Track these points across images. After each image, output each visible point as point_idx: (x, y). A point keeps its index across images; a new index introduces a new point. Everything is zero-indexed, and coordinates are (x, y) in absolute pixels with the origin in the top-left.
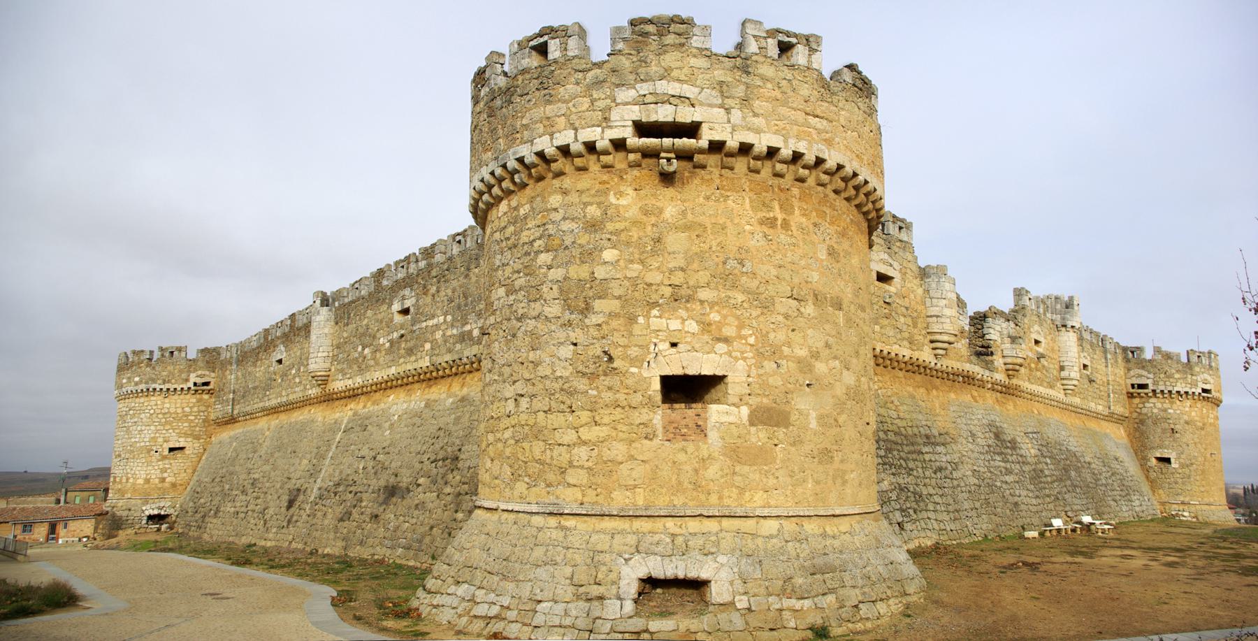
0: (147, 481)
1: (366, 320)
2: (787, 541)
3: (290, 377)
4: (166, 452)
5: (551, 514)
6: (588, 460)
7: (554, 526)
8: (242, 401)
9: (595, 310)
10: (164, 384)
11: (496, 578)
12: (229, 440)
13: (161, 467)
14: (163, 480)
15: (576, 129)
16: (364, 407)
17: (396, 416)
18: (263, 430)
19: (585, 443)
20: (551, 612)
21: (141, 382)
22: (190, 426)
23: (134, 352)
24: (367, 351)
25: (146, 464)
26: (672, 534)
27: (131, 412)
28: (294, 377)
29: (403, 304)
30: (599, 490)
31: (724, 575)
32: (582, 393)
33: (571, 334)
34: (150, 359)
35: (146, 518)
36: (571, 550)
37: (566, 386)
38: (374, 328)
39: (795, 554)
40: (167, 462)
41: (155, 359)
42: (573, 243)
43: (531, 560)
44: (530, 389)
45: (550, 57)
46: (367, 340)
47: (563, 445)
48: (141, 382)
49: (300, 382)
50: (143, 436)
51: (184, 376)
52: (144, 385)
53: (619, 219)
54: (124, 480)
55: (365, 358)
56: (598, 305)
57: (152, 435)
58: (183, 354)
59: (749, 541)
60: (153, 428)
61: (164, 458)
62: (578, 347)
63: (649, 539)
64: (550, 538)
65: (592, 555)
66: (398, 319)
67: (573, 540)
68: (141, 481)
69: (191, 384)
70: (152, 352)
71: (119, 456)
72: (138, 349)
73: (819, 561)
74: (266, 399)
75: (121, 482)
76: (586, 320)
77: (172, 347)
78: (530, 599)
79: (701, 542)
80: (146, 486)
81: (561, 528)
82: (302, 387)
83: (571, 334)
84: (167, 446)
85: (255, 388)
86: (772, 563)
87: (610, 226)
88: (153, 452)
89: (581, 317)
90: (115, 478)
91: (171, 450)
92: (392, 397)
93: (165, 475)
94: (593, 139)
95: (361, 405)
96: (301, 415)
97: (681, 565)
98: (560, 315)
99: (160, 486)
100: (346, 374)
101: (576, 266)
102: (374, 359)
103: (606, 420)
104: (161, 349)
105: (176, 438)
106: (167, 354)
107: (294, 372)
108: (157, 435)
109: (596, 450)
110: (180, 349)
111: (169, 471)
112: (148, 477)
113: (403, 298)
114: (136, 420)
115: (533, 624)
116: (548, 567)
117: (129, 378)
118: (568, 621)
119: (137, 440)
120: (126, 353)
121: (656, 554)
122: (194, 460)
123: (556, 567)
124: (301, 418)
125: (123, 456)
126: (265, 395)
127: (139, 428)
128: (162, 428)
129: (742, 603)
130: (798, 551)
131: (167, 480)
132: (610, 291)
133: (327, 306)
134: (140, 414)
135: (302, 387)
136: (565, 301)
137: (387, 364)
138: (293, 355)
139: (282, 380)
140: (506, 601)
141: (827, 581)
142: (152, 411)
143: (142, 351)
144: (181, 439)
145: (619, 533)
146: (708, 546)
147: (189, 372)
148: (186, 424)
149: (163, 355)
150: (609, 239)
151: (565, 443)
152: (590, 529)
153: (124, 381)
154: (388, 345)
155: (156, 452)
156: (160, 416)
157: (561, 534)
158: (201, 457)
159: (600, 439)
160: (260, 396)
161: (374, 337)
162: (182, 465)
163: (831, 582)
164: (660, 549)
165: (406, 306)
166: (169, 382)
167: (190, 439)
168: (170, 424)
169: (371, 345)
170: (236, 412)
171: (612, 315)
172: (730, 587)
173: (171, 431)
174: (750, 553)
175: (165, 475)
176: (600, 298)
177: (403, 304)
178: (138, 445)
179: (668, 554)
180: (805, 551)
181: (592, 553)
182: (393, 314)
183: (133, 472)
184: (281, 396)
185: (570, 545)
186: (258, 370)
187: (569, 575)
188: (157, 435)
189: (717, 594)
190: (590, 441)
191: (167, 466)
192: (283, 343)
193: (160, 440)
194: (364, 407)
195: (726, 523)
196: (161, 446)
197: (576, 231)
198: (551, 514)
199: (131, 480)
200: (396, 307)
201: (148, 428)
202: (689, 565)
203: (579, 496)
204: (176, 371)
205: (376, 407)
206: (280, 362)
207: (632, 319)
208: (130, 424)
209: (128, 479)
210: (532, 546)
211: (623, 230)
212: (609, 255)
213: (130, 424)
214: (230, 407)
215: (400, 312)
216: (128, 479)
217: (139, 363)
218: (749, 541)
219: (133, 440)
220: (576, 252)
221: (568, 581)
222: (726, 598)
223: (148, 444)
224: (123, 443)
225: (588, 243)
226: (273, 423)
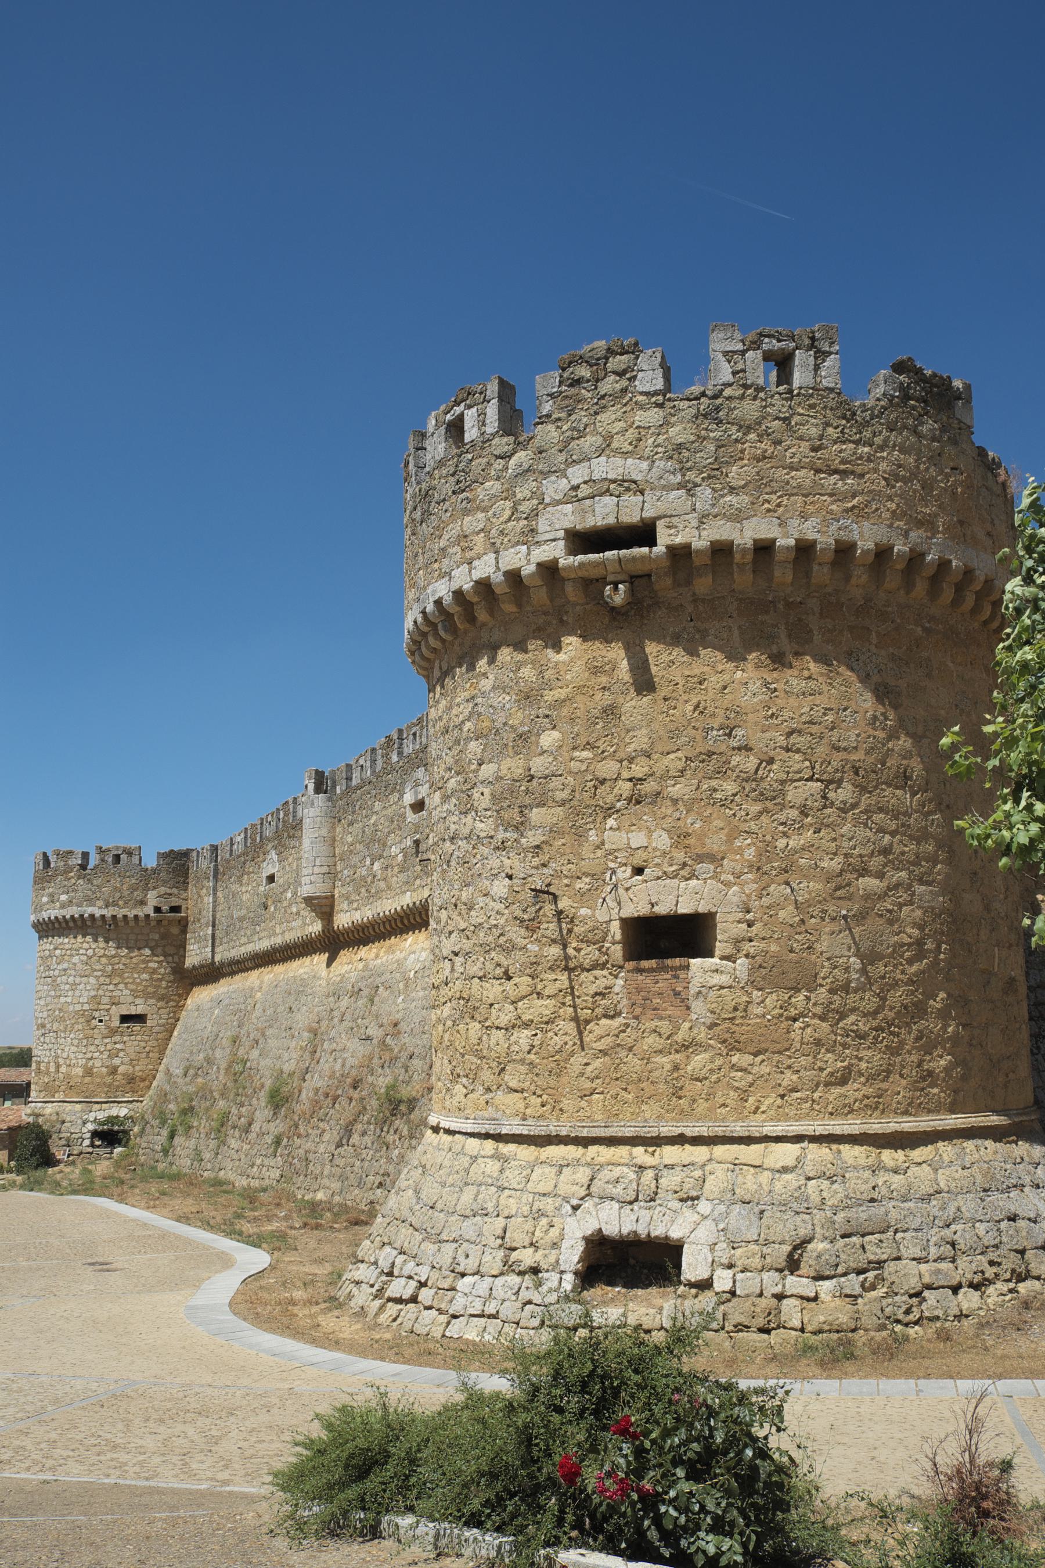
0: (89, 1072)
1: (374, 818)
2: (809, 1179)
3: (285, 904)
4: (116, 1022)
5: (487, 1136)
6: (529, 1052)
7: (490, 1153)
8: (225, 940)
9: (533, 824)
10: (107, 907)
11: (419, 1237)
12: (209, 1005)
13: (109, 1047)
14: (114, 1071)
15: (497, 552)
16: (377, 956)
17: (413, 972)
18: (252, 989)
19: (527, 1025)
20: (474, 1292)
21: (70, 902)
22: (151, 978)
23: (57, 853)
24: (377, 866)
25: (85, 1041)
26: (640, 1167)
27: (58, 952)
28: (290, 905)
29: (416, 793)
30: (545, 1097)
31: (706, 1233)
32: (520, 949)
33: (507, 862)
34: (83, 867)
35: (88, 1135)
36: (507, 1192)
37: (502, 940)
38: (384, 827)
39: (818, 1200)
40: (117, 1038)
41: (91, 866)
42: (505, 724)
43: (458, 1208)
44: (467, 945)
45: (467, 438)
46: (376, 848)
47: (501, 1029)
48: (70, 902)
49: (298, 913)
50: (77, 993)
51: (138, 895)
52: (75, 908)
53: (560, 684)
54: (52, 1069)
55: (374, 876)
56: (535, 815)
57: (93, 993)
58: (135, 860)
59: (749, 1177)
60: (92, 980)
61: (113, 1032)
62: (515, 881)
63: (606, 1174)
64: (483, 1173)
65: (531, 1200)
66: (411, 817)
67: (511, 1176)
68: (79, 1071)
69: (149, 910)
70: (85, 855)
71: (43, 1026)
72: (64, 848)
73: (862, 1214)
74: (256, 938)
75: (48, 1073)
76: (524, 841)
77: (117, 848)
78: (453, 1271)
79: (679, 1179)
80: (87, 1080)
81: (497, 1156)
82: (300, 922)
83: (507, 862)
84: (116, 1012)
85: (241, 919)
86: (778, 1214)
87: (550, 696)
88: (95, 1022)
89: (516, 836)
90: (39, 1063)
91: (125, 1019)
92: (410, 940)
93: (117, 1061)
94: (518, 566)
95: (372, 955)
96: (301, 966)
97: (645, 1215)
98: (493, 833)
99: (109, 1079)
100: (352, 902)
101: (508, 759)
102: (385, 879)
103: (550, 990)
104: (100, 850)
105: (130, 999)
106: (110, 859)
107: (289, 895)
108: (101, 992)
109: (539, 1036)
110: (130, 853)
111: (121, 1054)
112: (90, 1064)
113: (417, 784)
114: (65, 965)
115: (451, 1312)
116: (478, 1218)
117: (52, 895)
118: (491, 1309)
119: (69, 1000)
120: (45, 854)
121: (613, 1199)
122: (160, 1036)
123: (486, 1219)
124: (301, 971)
125: (48, 1026)
126: (255, 933)
127: (71, 980)
128: (108, 981)
129: (723, 1281)
130: (825, 1194)
131: (121, 1070)
132: (550, 794)
133: (326, 792)
134: (71, 956)
135: (300, 922)
136: (497, 811)
137: (400, 887)
138: (288, 868)
139: (275, 909)
140: (423, 1273)
141: (867, 1247)
142: (90, 952)
143: (71, 852)
144: (138, 1001)
145: (568, 1165)
146: (686, 1186)
147: (146, 889)
148: (145, 976)
149: (103, 860)
150: (547, 716)
151: (502, 1025)
152: (532, 1158)
153: (45, 899)
154: (400, 857)
155: (101, 1021)
156: (104, 960)
157: (497, 1165)
158: (172, 1032)
159: (545, 1019)
160: (249, 933)
161: (384, 845)
162: (143, 1044)
163: (874, 1248)
164: (618, 1190)
165: (420, 797)
166: (115, 904)
167: (151, 1001)
168: (121, 976)
169: (381, 857)
170: (217, 958)
171: (554, 831)
172: (709, 1255)
173: (121, 986)
174: (747, 1198)
175: (117, 1061)
176: (538, 806)
177: (416, 793)
178: (71, 1008)
179: (628, 1199)
180: (835, 1194)
181: (531, 1196)
182: (405, 808)
183: (65, 1055)
184: (275, 934)
185: (506, 1184)
186: (244, 889)
187: (499, 1232)
188: (101, 992)
189: (689, 1265)
190: (532, 1021)
191: (118, 1046)
192: (275, 848)
193: (105, 1000)
194: (377, 956)
195: (720, 1151)
196: (108, 1010)
197: (507, 706)
198: (487, 1136)
199: (63, 1069)
200: (409, 798)
201: (84, 980)
202: (655, 1217)
203: (521, 1105)
204: (125, 887)
205: (391, 957)
206: (271, 879)
207: (580, 836)
208: (57, 973)
209: (58, 1066)
210: (461, 1185)
211: (564, 701)
212: (549, 739)
213: (57, 973)
214: (209, 949)
215: (412, 806)
216: (58, 1066)
217: (66, 872)
218: (749, 1177)
219: (62, 1000)
220: (509, 737)
221: (499, 1241)
222: (703, 1274)
223: (86, 1007)
224: (47, 1005)
225: (522, 723)
226: (267, 978)
